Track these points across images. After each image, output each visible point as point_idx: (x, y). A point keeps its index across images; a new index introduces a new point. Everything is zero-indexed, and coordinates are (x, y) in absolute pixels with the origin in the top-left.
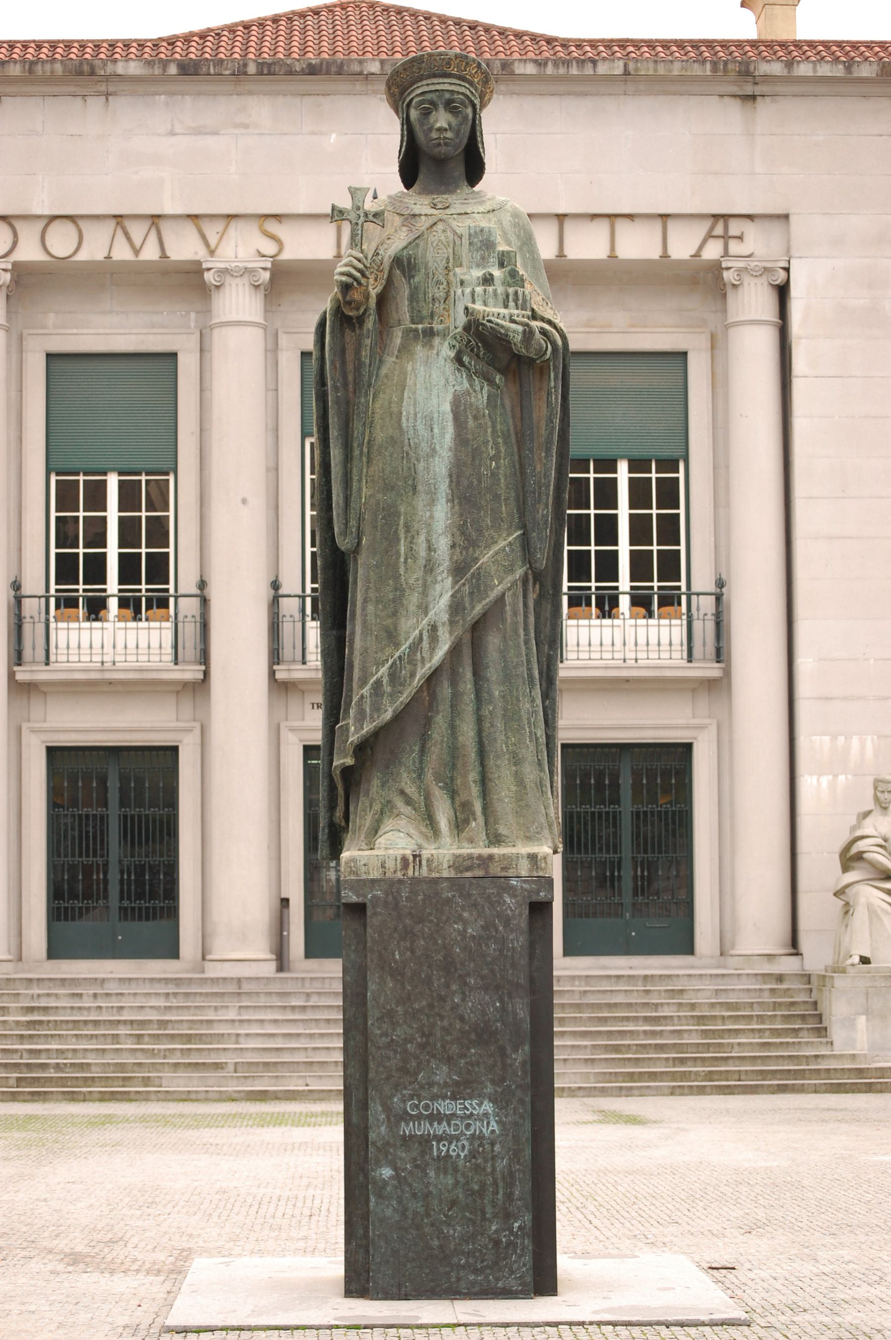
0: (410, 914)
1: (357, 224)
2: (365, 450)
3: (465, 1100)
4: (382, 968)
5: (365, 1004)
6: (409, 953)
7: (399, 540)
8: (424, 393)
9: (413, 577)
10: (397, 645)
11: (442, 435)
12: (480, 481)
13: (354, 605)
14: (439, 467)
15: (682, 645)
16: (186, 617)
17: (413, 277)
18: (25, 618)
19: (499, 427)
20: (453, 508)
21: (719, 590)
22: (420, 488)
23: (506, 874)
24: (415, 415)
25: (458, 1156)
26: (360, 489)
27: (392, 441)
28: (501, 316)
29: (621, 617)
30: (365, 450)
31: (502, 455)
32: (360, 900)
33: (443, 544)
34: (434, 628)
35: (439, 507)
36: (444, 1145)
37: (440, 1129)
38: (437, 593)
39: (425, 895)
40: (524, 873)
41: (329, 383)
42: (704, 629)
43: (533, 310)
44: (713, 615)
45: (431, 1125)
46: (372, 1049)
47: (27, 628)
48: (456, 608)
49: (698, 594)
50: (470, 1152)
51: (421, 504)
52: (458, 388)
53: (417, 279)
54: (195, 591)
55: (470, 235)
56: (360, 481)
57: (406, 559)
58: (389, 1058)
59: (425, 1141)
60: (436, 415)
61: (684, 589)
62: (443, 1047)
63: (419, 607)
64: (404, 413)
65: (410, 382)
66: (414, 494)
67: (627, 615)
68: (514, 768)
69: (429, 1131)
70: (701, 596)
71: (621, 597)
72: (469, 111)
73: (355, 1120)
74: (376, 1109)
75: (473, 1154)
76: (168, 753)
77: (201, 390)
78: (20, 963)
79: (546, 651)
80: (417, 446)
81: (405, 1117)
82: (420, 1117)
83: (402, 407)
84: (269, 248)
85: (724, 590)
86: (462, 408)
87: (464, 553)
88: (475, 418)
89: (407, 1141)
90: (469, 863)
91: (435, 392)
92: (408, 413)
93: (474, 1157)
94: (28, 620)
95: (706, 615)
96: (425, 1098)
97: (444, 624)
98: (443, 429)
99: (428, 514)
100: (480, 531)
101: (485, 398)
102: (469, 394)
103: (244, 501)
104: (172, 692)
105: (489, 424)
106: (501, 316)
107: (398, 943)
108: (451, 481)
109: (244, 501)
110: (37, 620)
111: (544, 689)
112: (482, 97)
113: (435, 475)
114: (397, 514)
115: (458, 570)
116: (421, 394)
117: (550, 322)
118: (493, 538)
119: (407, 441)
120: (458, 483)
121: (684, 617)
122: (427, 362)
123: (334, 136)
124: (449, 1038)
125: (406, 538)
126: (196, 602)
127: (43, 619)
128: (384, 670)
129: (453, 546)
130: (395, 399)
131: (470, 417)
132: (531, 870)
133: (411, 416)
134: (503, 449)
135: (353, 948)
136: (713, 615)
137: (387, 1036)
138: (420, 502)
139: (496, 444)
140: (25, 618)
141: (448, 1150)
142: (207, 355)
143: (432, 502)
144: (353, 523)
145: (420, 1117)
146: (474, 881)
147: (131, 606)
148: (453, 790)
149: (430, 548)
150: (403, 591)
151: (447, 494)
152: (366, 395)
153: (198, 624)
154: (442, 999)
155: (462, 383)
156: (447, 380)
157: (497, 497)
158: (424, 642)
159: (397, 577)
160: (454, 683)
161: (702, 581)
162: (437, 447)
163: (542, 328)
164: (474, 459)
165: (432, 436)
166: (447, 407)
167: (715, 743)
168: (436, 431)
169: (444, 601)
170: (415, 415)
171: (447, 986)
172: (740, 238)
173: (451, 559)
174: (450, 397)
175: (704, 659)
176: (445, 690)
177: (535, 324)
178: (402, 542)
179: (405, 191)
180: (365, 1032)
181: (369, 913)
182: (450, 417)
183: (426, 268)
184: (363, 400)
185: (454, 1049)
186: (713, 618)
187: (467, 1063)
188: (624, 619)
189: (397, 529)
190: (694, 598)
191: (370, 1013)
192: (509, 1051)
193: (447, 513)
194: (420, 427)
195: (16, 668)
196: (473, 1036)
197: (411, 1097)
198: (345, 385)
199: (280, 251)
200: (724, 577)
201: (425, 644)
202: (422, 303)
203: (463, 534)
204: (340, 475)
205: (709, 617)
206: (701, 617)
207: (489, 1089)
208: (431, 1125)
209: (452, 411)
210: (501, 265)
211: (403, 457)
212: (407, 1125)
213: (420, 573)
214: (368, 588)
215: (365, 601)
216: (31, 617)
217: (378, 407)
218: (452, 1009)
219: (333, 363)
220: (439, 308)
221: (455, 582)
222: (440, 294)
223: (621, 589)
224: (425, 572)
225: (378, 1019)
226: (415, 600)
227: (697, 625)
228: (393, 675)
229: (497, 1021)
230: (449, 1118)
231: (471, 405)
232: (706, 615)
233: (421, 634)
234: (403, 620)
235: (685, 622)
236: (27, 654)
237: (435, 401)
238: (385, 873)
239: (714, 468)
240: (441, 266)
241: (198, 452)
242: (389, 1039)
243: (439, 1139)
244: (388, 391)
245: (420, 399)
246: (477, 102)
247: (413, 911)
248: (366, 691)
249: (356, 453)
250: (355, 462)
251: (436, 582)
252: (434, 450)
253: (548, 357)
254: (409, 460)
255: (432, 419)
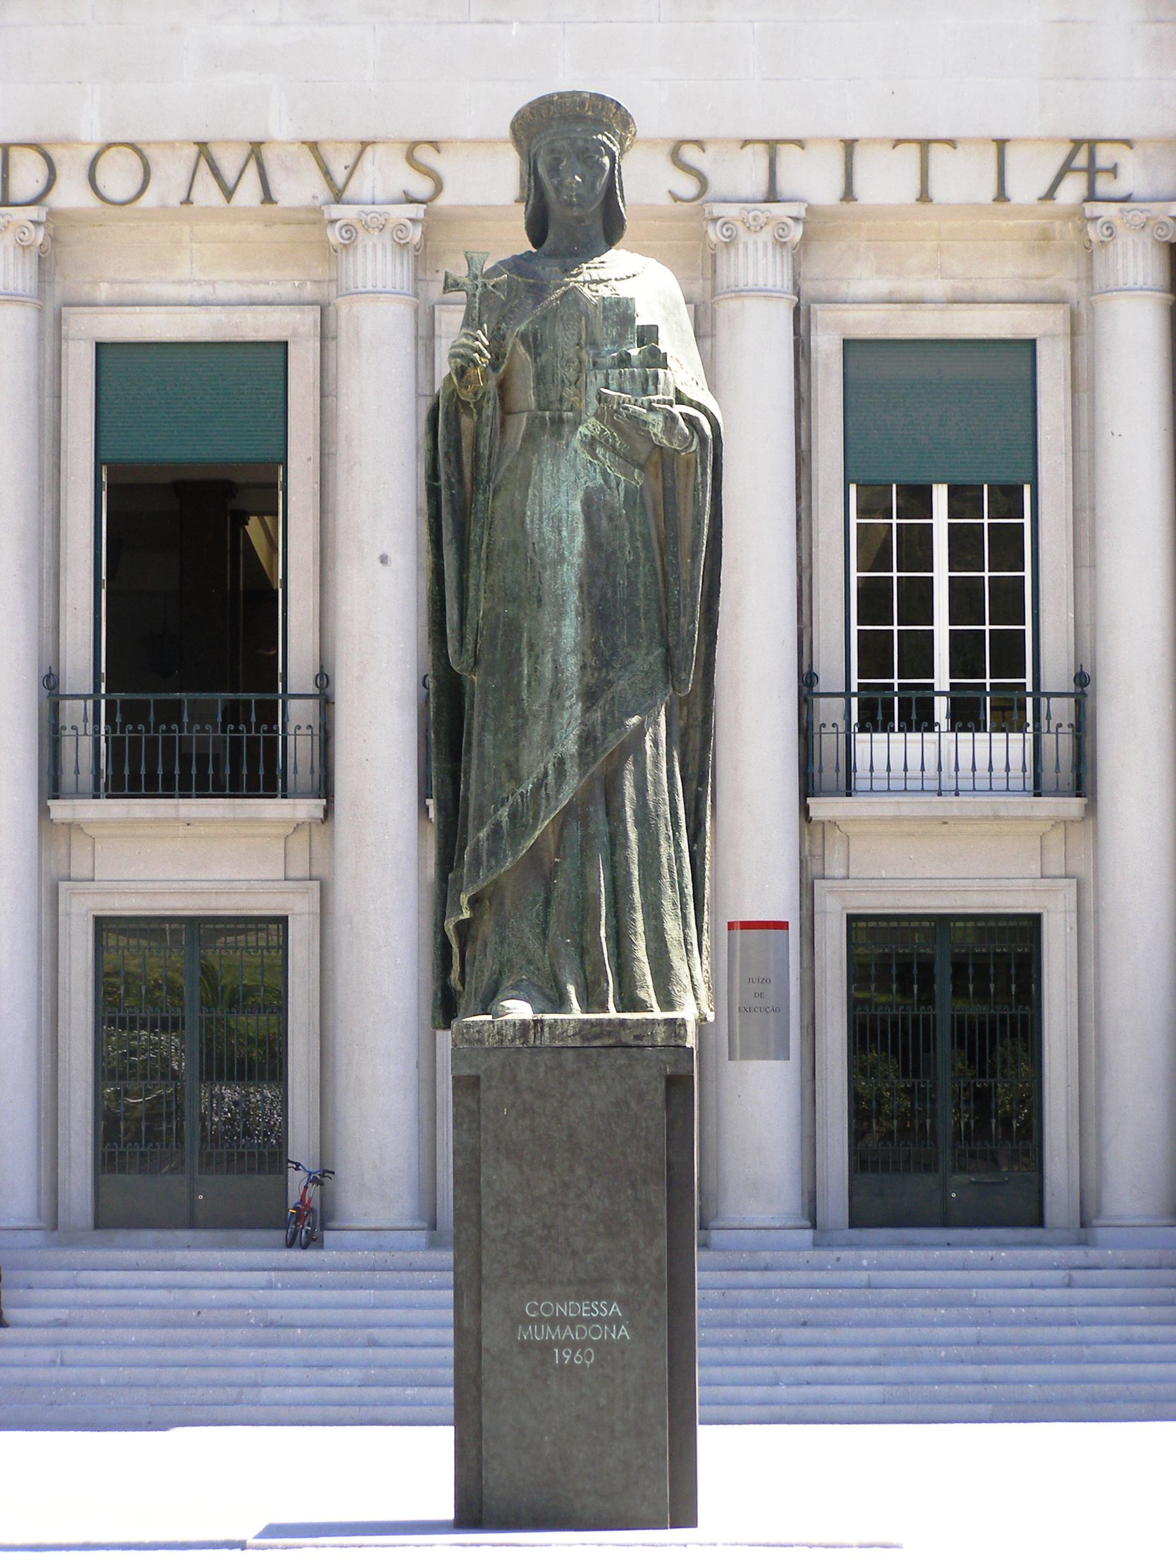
0: (530, 1088)
1: (474, 295)
2: (483, 555)
3: (591, 1300)
4: (498, 1149)
5: (479, 1192)
6: (528, 1132)
7: (521, 660)
8: (551, 490)
9: (536, 703)
10: (519, 782)
11: (572, 540)
12: (615, 592)
13: (469, 734)
14: (570, 574)
15: (1024, 770)
16: (299, 727)
17: (540, 355)
18: (64, 728)
19: (637, 529)
20: (583, 623)
21: (1079, 690)
22: (546, 599)
23: (640, 1043)
24: (541, 515)
25: (584, 1364)
26: (477, 601)
27: (515, 546)
28: (639, 402)
29: (937, 729)
30: (483, 555)
31: (642, 561)
32: (473, 1072)
33: (572, 666)
34: (561, 762)
35: (568, 622)
36: (567, 1353)
37: (559, 1334)
38: (565, 721)
39: (546, 1066)
40: (659, 1041)
41: (443, 477)
42: (1058, 746)
43: (677, 391)
44: (1070, 725)
45: (553, 1330)
46: (486, 1242)
47: (68, 744)
48: (587, 739)
49: (1050, 695)
50: (596, 1360)
51: (547, 618)
52: (589, 484)
53: (544, 357)
54: (311, 689)
55: (604, 308)
56: (478, 590)
57: (529, 683)
58: (505, 1253)
59: (546, 1347)
60: (565, 515)
61: (1029, 689)
62: (567, 1240)
63: (544, 737)
64: (529, 513)
65: (535, 478)
66: (539, 607)
67: (944, 727)
68: (653, 922)
69: (550, 1337)
70: (1052, 700)
71: (937, 699)
72: (606, 160)
73: (466, 1324)
74: (492, 1310)
75: (599, 1363)
76: (273, 927)
77: (322, 396)
78: (55, 1233)
79: (694, 787)
80: (543, 550)
81: (526, 1321)
82: (540, 1320)
83: (525, 506)
84: (421, 187)
85: (1087, 689)
86: (595, 507)
87: (596, 674)
88: (611, 519)
89: (526, 1347)
90: (597, 1029)
91: (564, 488)
92: (533, 514)
93: (602, 1366)
94: (68, 731)
95: (1060, 725)
96: (546, 1299)
97: (572, 756)
98: (572, 531)
99: (555, 629)
100: (614, 652)
101: (622, 495)
102: (603, 491)
103: (384, 560)
104: (277, 837)
105: (627, 525)
106: (639, 402)
107: (516, 1120)
108: (582, 592)
109: (384, 560)
110: (81, 732)
111: (691, 832)
112: (621, 144)
113: (563, 584)
114: (519, 630)
115: (590, 697)
116: (548, 490)
117: (699, 407)
118: (629, 657)
119: (531, 546)
120: (590, 593)
121: (1030, 729)
122: (556, 455)
123: (515, 25)
124: (572, 1230)
125: (530, 657)
126: (312, 705)
127: (90, 731)
128: (504, 812)
129: (583, 667)
130: (518, 496)
131: (604, 517)
132: (669, 1037)
133: (537, 516)
134: (642, 554)
135: (465, 1127)
136: (1070, 725)
137: (502, 1226)
138: (546, 615)
139: (635, 549)
140: (64, 728)
141: (572, 1358)
142: (331, 345)
143: (560, 616)
144: (470, 638)
145: (540, 1320)
146: (603, 1051)
147: (965, 716)
148: (582, 947)
149: (557, 669)
150: (526, 719)
151: (577, 607)
152: (485, 491)
153: (316, 739)
154: (566, 1185)
155: (595, 478)
156: (578, 474)
157: (635, 610)
158: (550, 778)
159: (518, 701)
160: (585, 825)
161: (1056, 673)
162: (566, 553)
163: (687, 415)
164: (608, 566)
165: (561, 540)
166: (577, 506)
167: (1074, 915)
168: (564, 533)
169: (574, 733)
170: (541, 515)
171: (572, 1170)
172: (1113, 171)
173: (581, 682)
174: (580, 494)
175: (1024, 790)
176: (575, 832)
177: (677, 409)
178: (525, 661)
179: (534, 250)
180: (478, 1224)
181: (483, 1087)
182: (580, 517)
183: (555, 344)
184: (481, 498)
185: (579, 1243)
186: (1070, 730)
187: (594, 1259)
188: (940, 732)
189: (518, 649)
190: (1044, 700)
191: (483, 1201)
192: (642, 1246)
193: (576, 629)
194: (547, 530)
195: (50, 803)
196: (601, 1229)
197: (531, 1298)
198: (461, 481)
199: (439, 187)
200: (1087, 670)
201: (551, 779)
202: (550, 385)
203: (594, 653)
204: (455, 584)
205: (1065, 729)
206: (1053, 729)
207: (619, 1289)
208: (553, 1330)
209: (583, 511)
210: (641, 343)
211: (526, 565)
212: (526, 1329)
213: (545, 698)
214: (486, 715)
215: (483, 728)
216: (74, 728)
217: (499, 505)
218: (578, 1196)
219: (446, 454)
220: (569, 391)
221: (587, 709)
222: (571, 374)
223: (937, 689)
224: (552, 696)
225: (492, 1208)
226: (539, 728)
227: (1048, 740)
228: (513, 816)
229: (627, 1210)
230: (573, 1322)
231: (605, 504)
232: (1060, 725)
233: (546, 769)
234: (525, 752)
235: (1030, 737)
236: (68, 778)
237: (563, 498)
238: (502, 1041)
239: (1074, 510)
240: (572, 343)
241: (317, 486)
242: (505, 1231)
243: (562, 1345)
244: (510, 487)
245: (547, 497)
246: (616, 149)
247: (533, 1085)
248: (483, 834)
249: (473, 558)
250: (473, 571)
251: (563, 708)
252: (562, 556)
253: (693, 448)
254: (533, 569)
255: (560, 520)
